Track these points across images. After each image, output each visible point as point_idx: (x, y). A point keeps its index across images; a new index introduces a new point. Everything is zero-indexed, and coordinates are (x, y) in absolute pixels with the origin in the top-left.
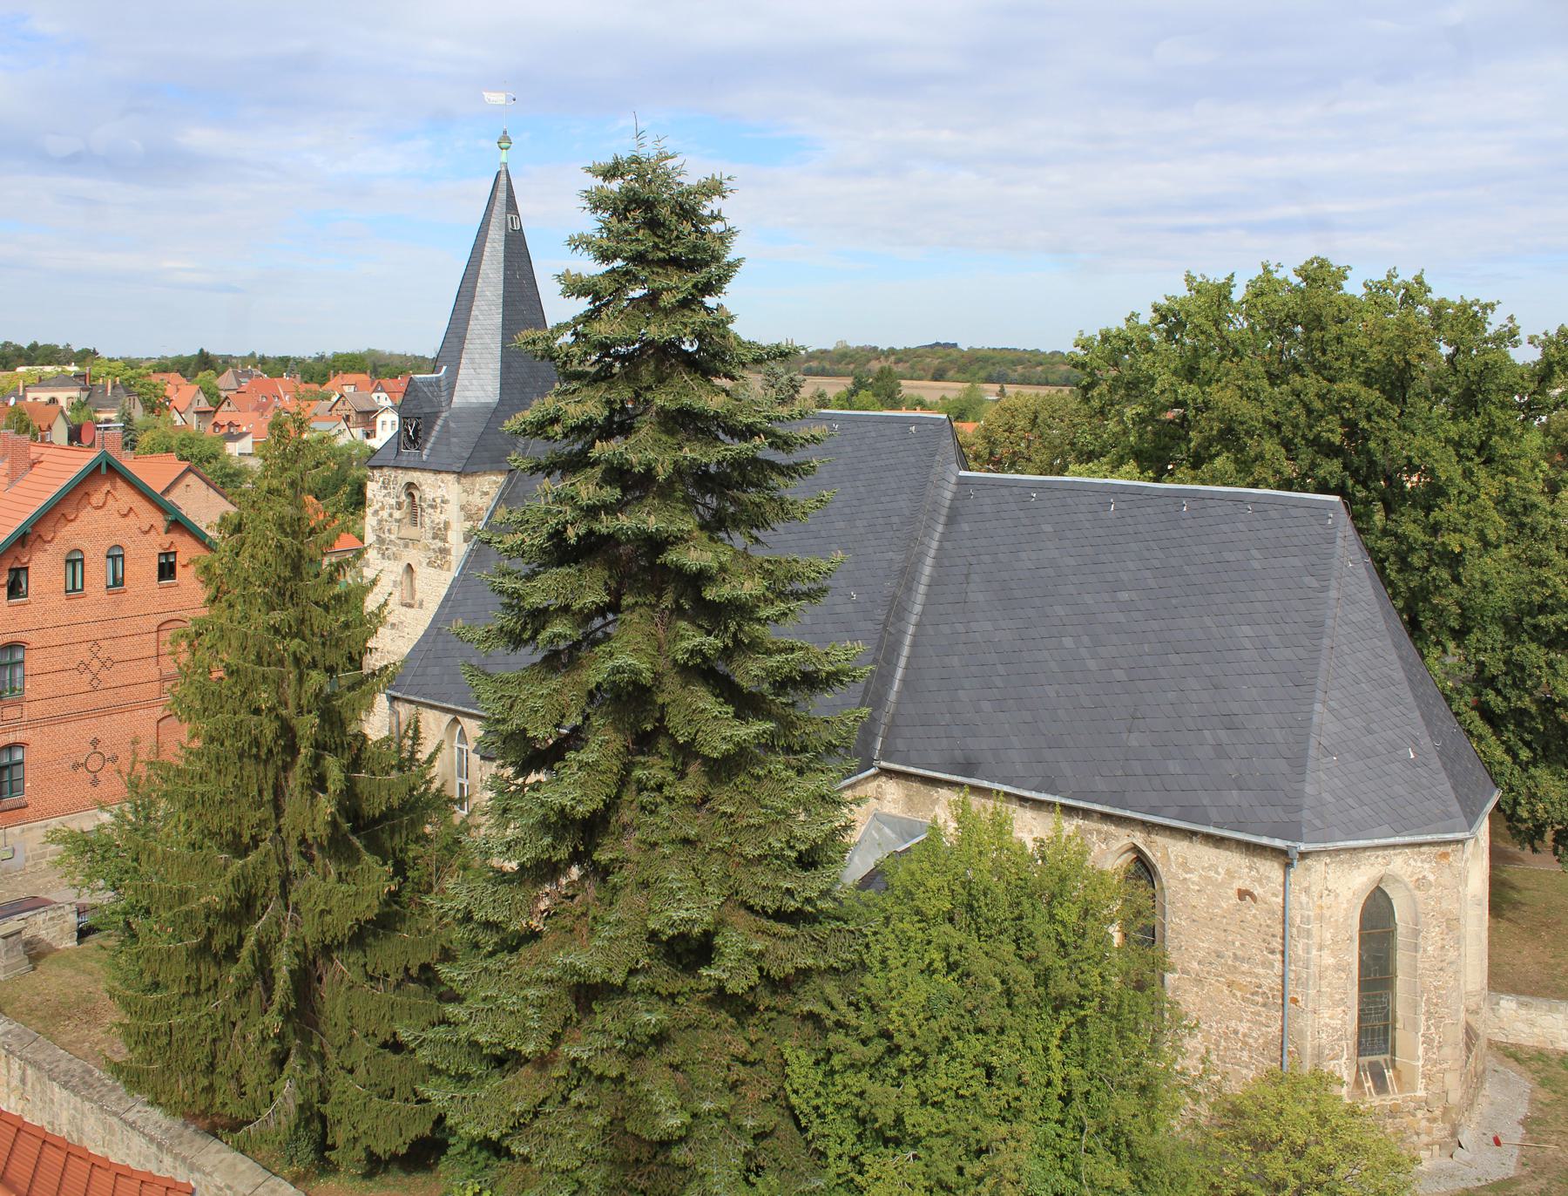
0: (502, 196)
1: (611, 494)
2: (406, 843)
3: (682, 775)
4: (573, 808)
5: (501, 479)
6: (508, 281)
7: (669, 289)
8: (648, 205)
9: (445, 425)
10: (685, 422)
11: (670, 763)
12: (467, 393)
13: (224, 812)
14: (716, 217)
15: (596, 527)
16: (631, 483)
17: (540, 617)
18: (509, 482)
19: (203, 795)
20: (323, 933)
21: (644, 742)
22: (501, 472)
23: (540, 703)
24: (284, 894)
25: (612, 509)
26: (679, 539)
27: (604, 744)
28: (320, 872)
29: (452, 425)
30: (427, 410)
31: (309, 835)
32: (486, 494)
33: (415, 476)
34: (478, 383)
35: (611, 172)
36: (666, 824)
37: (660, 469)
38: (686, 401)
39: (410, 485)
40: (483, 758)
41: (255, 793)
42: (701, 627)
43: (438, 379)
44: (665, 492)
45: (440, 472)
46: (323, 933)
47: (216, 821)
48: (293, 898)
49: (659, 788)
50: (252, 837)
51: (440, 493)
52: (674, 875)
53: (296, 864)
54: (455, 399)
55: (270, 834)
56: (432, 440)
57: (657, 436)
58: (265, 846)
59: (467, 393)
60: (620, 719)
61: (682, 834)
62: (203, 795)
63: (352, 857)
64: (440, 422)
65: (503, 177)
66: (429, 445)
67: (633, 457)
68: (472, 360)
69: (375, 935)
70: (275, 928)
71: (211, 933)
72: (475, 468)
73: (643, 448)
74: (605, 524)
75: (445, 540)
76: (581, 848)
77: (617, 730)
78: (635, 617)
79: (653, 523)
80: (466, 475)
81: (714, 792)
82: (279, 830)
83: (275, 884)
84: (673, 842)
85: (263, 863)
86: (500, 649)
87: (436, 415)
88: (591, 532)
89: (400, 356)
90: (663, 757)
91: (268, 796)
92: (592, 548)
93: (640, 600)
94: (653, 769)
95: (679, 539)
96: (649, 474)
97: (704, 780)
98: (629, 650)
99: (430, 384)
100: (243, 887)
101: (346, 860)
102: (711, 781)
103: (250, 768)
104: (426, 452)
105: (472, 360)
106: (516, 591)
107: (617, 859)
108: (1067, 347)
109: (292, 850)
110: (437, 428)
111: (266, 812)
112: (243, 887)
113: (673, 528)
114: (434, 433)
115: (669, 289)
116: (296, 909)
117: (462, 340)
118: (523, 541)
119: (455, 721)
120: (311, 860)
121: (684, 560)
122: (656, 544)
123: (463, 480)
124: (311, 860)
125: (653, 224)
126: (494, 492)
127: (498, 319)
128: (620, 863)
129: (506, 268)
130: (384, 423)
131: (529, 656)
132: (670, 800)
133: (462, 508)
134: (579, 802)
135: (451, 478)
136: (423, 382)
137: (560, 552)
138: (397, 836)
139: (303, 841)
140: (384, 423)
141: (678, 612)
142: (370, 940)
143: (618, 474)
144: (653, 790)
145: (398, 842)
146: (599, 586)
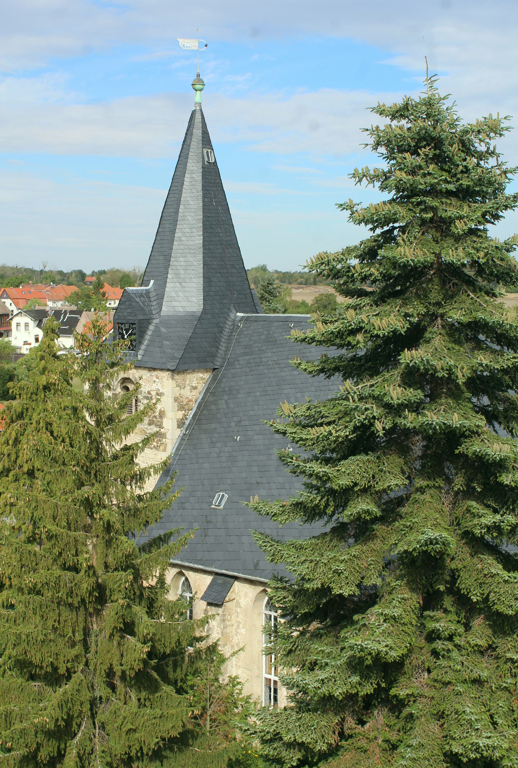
0: (197, 132)
1: (414, 394)
2: (186, 675)
3: (467, 627)
4: (387, 653)
5: (207, 376)
6: (206, 208)
7: (461, 218)
8: (437, 143)
9: (157, 330)
10: (471, 333)
11: (455, 617)
12: (175, 304)
13: (45, 650)
14: (491, 153)
15: (400, 421)
16: (431, 384)
17: (343, 496)
18: (214, 379)
19: (28, 636)
20: (130, 747)
21: (431, 601)
22: (206, 370)
23: (342, 567)
24: (93, 716)
25: (416, 408)
26: (475, 433)
27: (401, 601)
28: (122, 697)
29: (163, 330)
30: (141, 317)
31: (118, 669)
32: (195, 388)
33: (133, 374)
34: (184, 295)
35: (401, 112)
36: (459, 667)
37: (460, 375)
38: (480, 315)
39: (126, 380)
40: (209, 604)
41: (70, 634)
42: (488, 506)
43: (148, 292)
44: (455, 393)
45: (154, 369)
46: (130, 747)
47: (39, 656)
48: (100, 717)
49: (450, 638)
50: (68, 670)
51: (154, 387)
52: (470, 710)
53: (101, 691)
54: (164, 308)
55: (81, 667)
56: (146, 342)
57: (450, 345)
58: (77, 677)
59: (175, 304)
60: (413, 581)
61: (475, 675)
62: (28, 636)
63: (154, 688)
64: (151, 327)
65: (198, 117)
66: (143, 347)
67: (438, 364)
68: (177, 275)
69: (172, 750)
70: (88, 743)
71: (39, 746)
72: (186, 366)
73: (434, 353)
74: (410, 420)
75: (160, 426)
76: (383, 685)
77: (412, 590)
78: (426, 497)
79: (455, 420)
80: (179, 373)
81: (499, 641)
82: (87, 664)
83: (86, 707)
84: (465, 681)
85: (78, 691)
86: (298, 520)
87: (148, 321)
88: (395, 425)
89: (12, 268)
90: (446, 611)
91: (79, 637)
92: (398, 440)
93: (431, 483)
94: (443, 622)
95: (475, 433)
96: (450, 379)
97: (489, 632)
98: (429, 523)
99: (141, 295)
100: (65, 710)
101: (145, 689)
102: (495, 632)
103: (66, 613)
104: (141, 352)
105: (177, 275)
106: (326, 474)
107: (412, 695)
108: (300, 269)
109: (99, 681)
110: (149, 333)
111: (78, 649)
112: (65, 710)
113: (467, 423)
114: (147, 337)
115: (461, 218)
116: (103, 727)
117: (167, 258)
118: (330, 433)
119: (181, 574)
120: (113, 687)
121: (489, 451)
122: (453, 437)
123: (176, 377)
124: (113, 687)
125: (441, 159)
126: (202, 387)
127: (199, 240)
128: (414, 697)
129: (204, 197)
130: (18, 325)
131: (320, 526)
132: (458, 647)
133: (176, 400)
134: (391, 648)
135: (165, 375)
136: (136, 293)
137: (363, 441)
138: (179, 669)
139: (110, 673)
140: (18, 325)
141: (469, 493)
142: (168, 753)
143: (413, 377)
144: (446, 639)
145: (179, 674)
146: (397, 471)
